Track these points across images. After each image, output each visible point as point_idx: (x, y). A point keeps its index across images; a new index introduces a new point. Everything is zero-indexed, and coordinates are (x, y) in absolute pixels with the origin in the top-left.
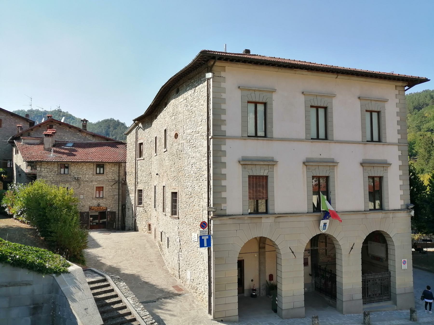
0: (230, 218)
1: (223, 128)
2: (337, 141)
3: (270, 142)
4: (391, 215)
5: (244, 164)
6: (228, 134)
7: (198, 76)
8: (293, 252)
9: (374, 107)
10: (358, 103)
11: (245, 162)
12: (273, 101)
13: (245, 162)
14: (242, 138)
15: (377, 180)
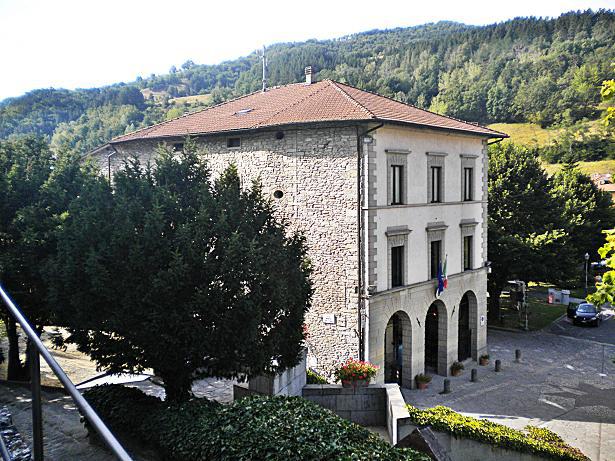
7: (332, 130)
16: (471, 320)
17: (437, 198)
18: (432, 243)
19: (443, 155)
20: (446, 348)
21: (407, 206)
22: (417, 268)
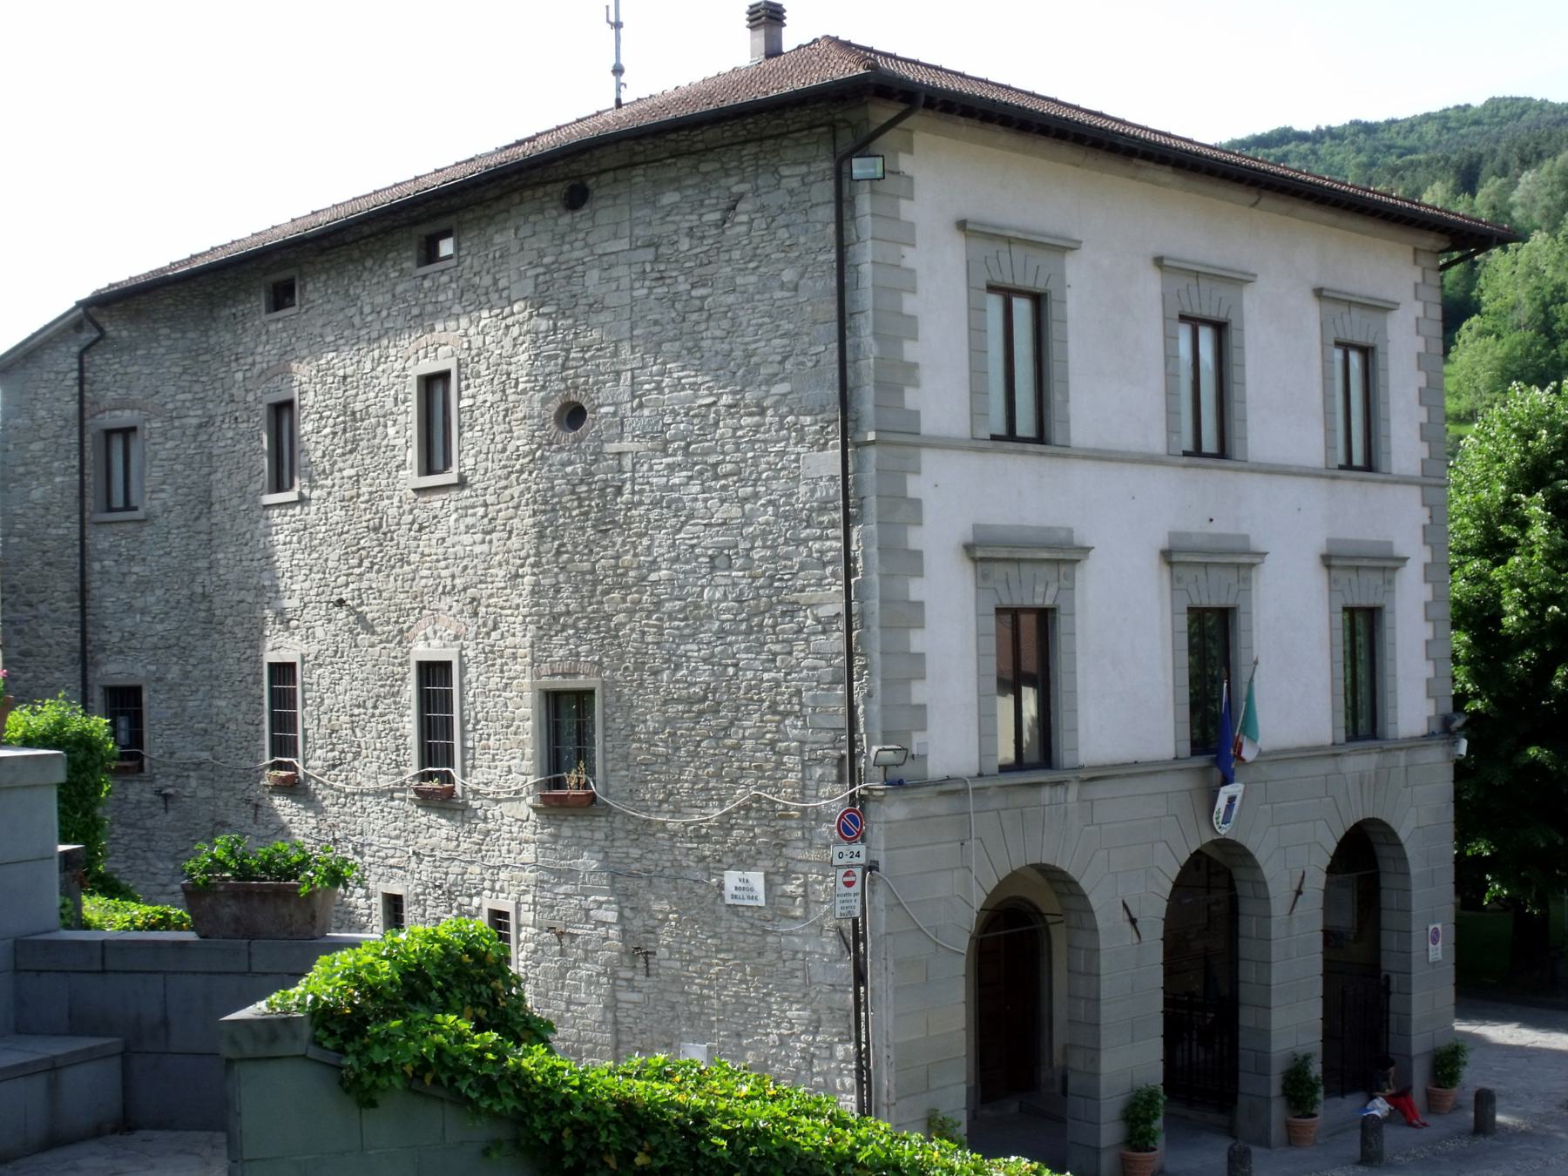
0: (942, 793)
1: (911, 398)
2: (1259, 464)
3: (1060, 462)
4: (1402, 758)
5: (982, 560)
6: (927, 427)
7: (751, 149)
8: (1133, 921)
9: (1023, 270)
10: (1312, 312)
11: (984, 553)
12: (1068, 292)
13: (984, 553)
14: (974, 444)
15: (1028, 623)
16: (1389, 941)
17: (1213, 437)
18: (1351, 612)
19: (1238, 280)
20: (1265, 1034)
21: (1067, 453)
22: (1124, 695)
